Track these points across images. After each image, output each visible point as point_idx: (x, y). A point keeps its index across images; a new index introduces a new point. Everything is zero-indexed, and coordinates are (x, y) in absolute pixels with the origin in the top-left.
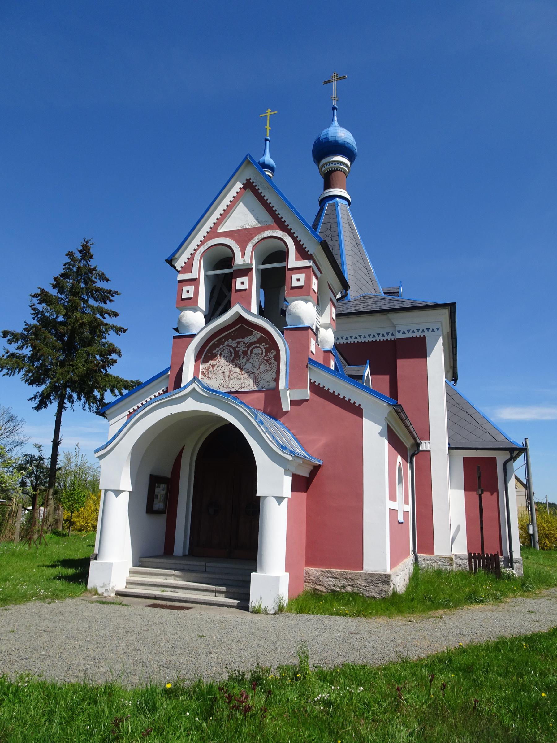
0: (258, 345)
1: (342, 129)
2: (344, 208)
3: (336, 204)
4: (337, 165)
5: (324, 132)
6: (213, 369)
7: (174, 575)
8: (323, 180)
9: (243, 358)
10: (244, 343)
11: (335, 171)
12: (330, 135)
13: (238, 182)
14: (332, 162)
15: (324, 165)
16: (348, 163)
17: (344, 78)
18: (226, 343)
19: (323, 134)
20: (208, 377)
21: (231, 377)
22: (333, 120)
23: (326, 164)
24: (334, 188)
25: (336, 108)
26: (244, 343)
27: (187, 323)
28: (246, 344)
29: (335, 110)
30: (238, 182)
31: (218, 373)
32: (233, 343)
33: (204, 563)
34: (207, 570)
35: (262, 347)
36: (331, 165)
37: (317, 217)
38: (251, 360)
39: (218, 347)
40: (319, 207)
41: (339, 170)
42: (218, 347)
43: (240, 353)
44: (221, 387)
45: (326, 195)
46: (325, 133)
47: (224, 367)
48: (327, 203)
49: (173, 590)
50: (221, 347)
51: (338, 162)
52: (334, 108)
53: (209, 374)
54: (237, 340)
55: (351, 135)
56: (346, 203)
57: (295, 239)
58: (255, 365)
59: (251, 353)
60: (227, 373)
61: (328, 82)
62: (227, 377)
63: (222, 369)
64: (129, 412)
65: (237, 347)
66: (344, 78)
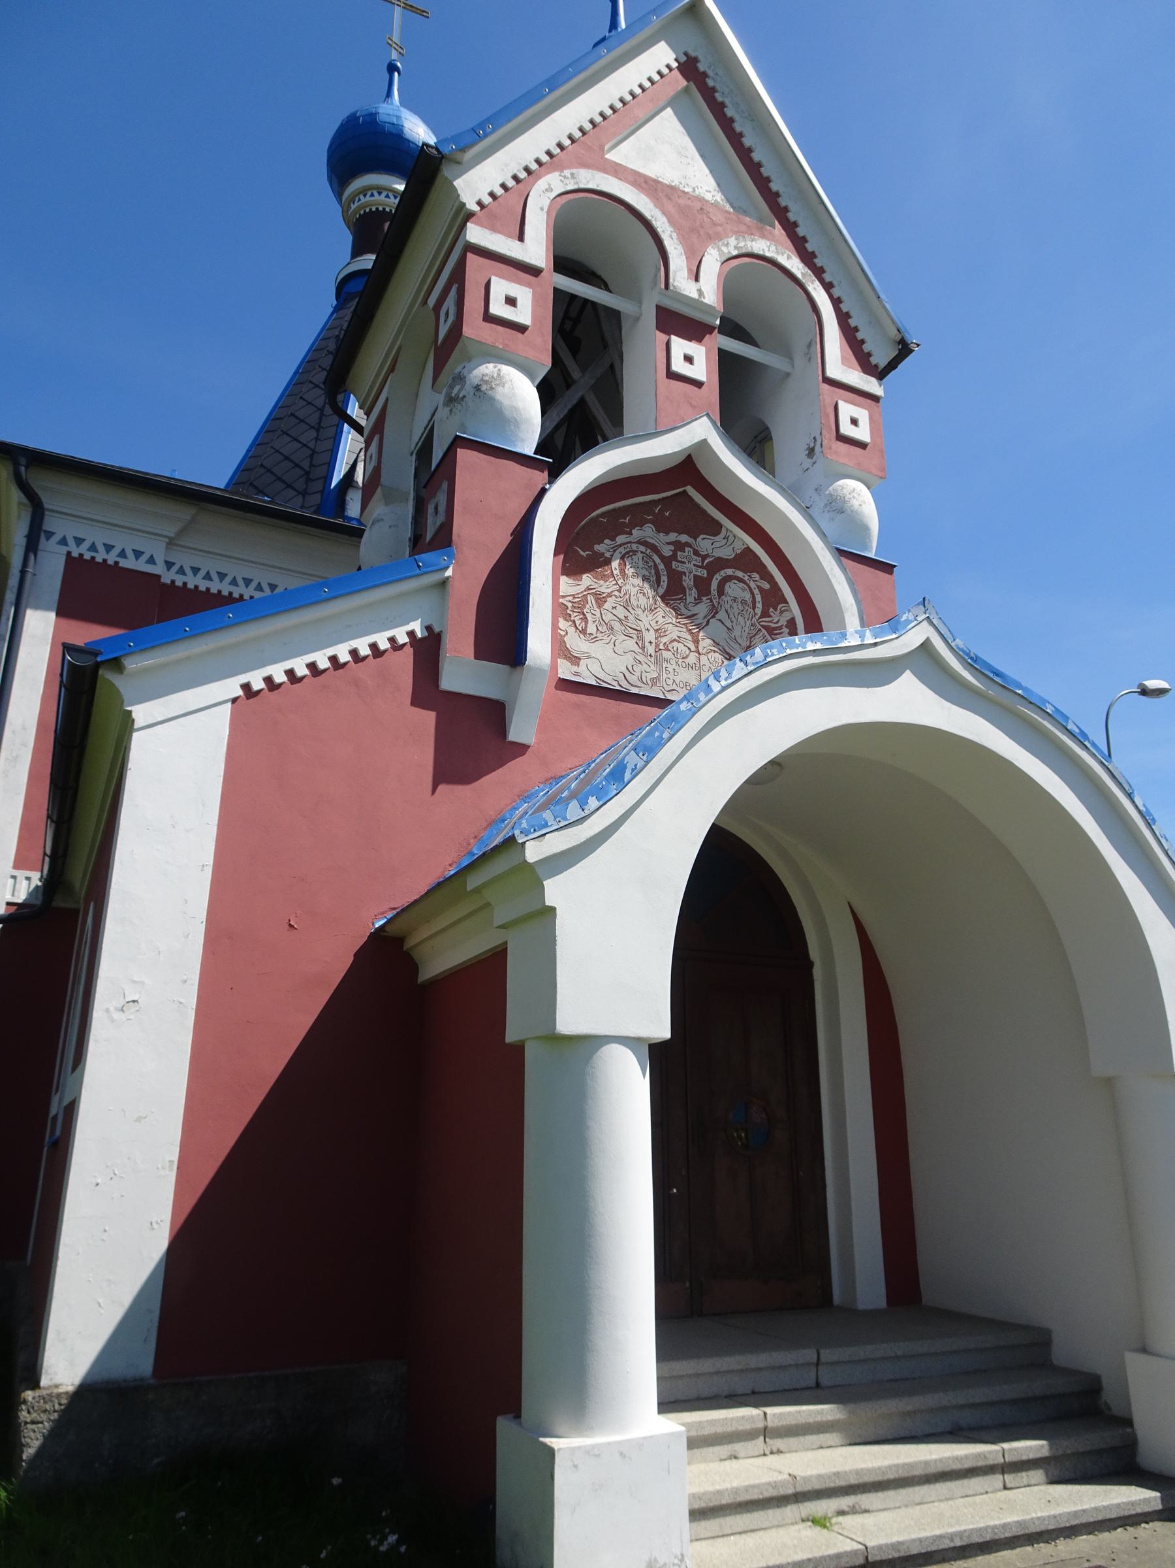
0: (740, 574)
6: (599, 607)
7: (766, 1433)
9: (698, 601)
10: (696, 553)
13: (662, 45)
15: (371, 188)
18: (637, 533)
20: (584, 632)
21: (666, 654)
26: (696, 553)
27: (516, 409)
28: (704, 557)
30: (662, 45)
31: (617, 626)
32: (664, 541)
33: (809, 1355)
34: (825, 1381)
35: (752, 585)
38: (722, 615)
39: (613, 539)
42: (613, 539)
43: (688, 582)
44: (633, 679)
47: (639, 611)
49: (845, 1502)
50: (621, 539)
53: (585, 619)
54: (673, 537)
57: (836, 302)
58: (737, 633)
59: (721, 591)
60: (650, 636)
62: (651, 650)
63: (631, 618)
64: (246, 687)
65: (674, 557)
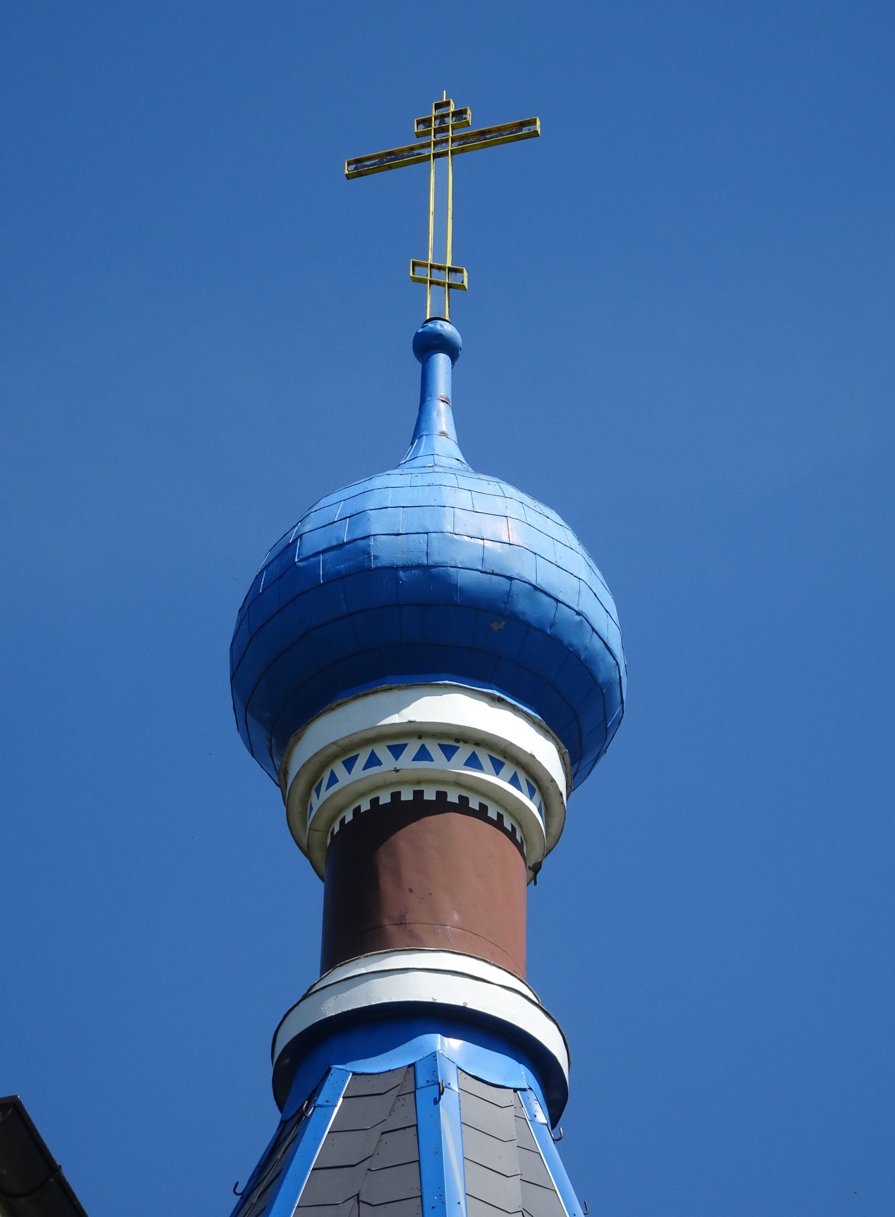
1: (490, 485)
2: (504, 1122)
3: (423, 1084)
4: (458, 767)
5: (333, 506)
8: (317, 888)
11: (420, 808)
12: (377, 525)
14: (398, 739)
16: (546, 753)
17: (520, 130)
19: (324, 521)
22: (419, 429)
23: (346, 753)
24: (416, 945)
25: (452, 350)
29: (442, 361)
36: (344, 778)
37: (245, 1197)
40: (276, 1116)
41: (462, 807)
45: (333, 1006)
46: (337, 512)
48: (342, 1079)
51: (453, 739)
52: (428, 345)
55: (569, 537)
56: (521, 1075)
61: (389, 160)
66: (520, 130)
